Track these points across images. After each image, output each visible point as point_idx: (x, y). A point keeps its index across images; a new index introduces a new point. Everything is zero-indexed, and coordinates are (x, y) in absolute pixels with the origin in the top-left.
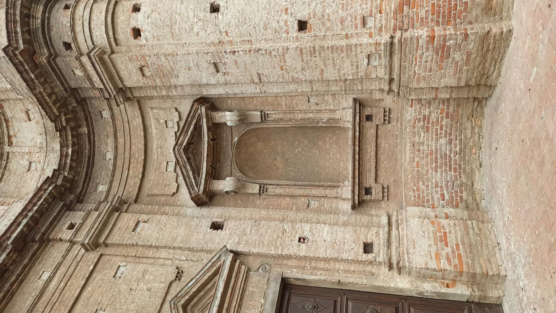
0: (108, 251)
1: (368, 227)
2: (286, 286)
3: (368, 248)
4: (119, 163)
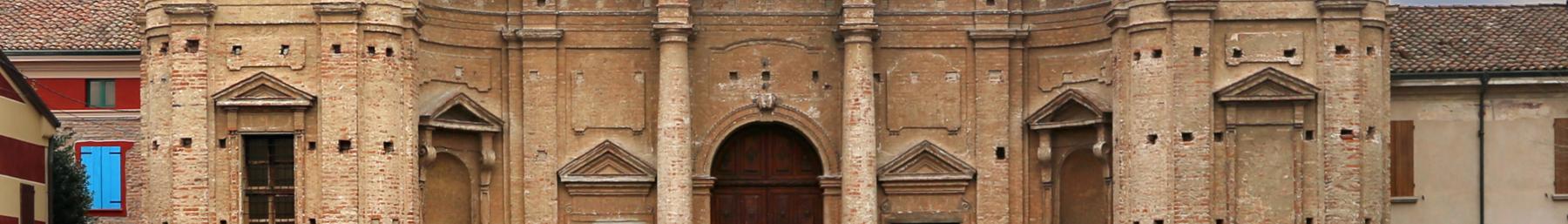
0: (970, 52)
4: (1068, 16)
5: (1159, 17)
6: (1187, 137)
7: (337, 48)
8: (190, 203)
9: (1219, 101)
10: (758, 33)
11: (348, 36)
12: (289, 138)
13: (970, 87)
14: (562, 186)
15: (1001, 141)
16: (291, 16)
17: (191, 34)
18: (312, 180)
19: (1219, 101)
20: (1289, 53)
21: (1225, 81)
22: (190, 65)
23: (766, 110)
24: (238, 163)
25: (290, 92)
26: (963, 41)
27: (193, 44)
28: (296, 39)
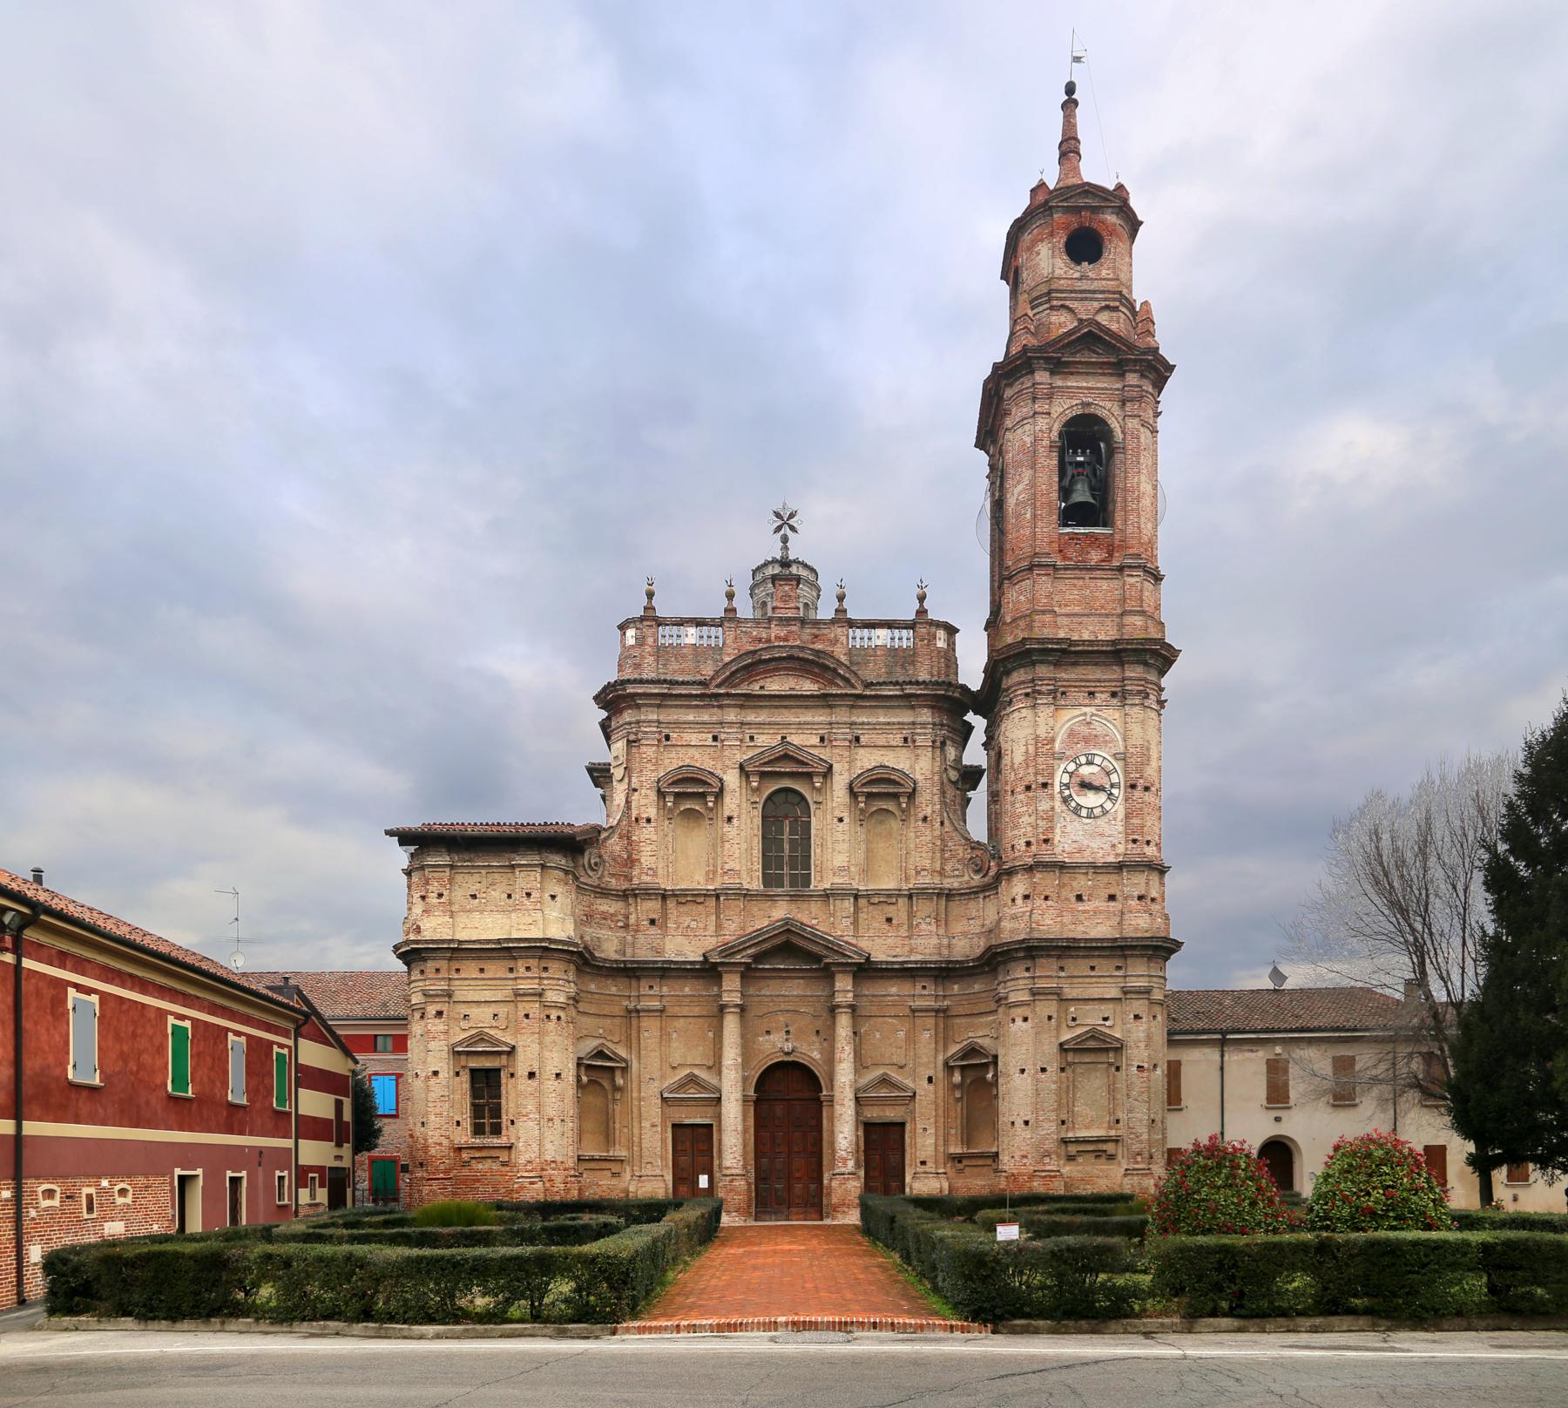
1: (936, 1162)
2: (903, 1125)
3: (923, 1163)
5: (1026, 997)
6: (1043, 1070)
7: (527, 1016)
8: (438, 1110)
9: (1063, 1048)
10: (783, 1007)
11: (534, 1008)
12: (498, 1070)
13: (911, 1040)
14: (664, 1099)
15: (931, 1073)
16: (499, 996)
17: (439, 1007)
18: (512, 1095)
19: (1063, 1048)
20: (1105, 1019)
21: (1066, 1036)
22: (437, 1026)
23: (788, 1054)
24: (467, 1086)
25: (498, 1042)
26: (907, 1012)
27: (439, 1014)
28: (502, 1010)
